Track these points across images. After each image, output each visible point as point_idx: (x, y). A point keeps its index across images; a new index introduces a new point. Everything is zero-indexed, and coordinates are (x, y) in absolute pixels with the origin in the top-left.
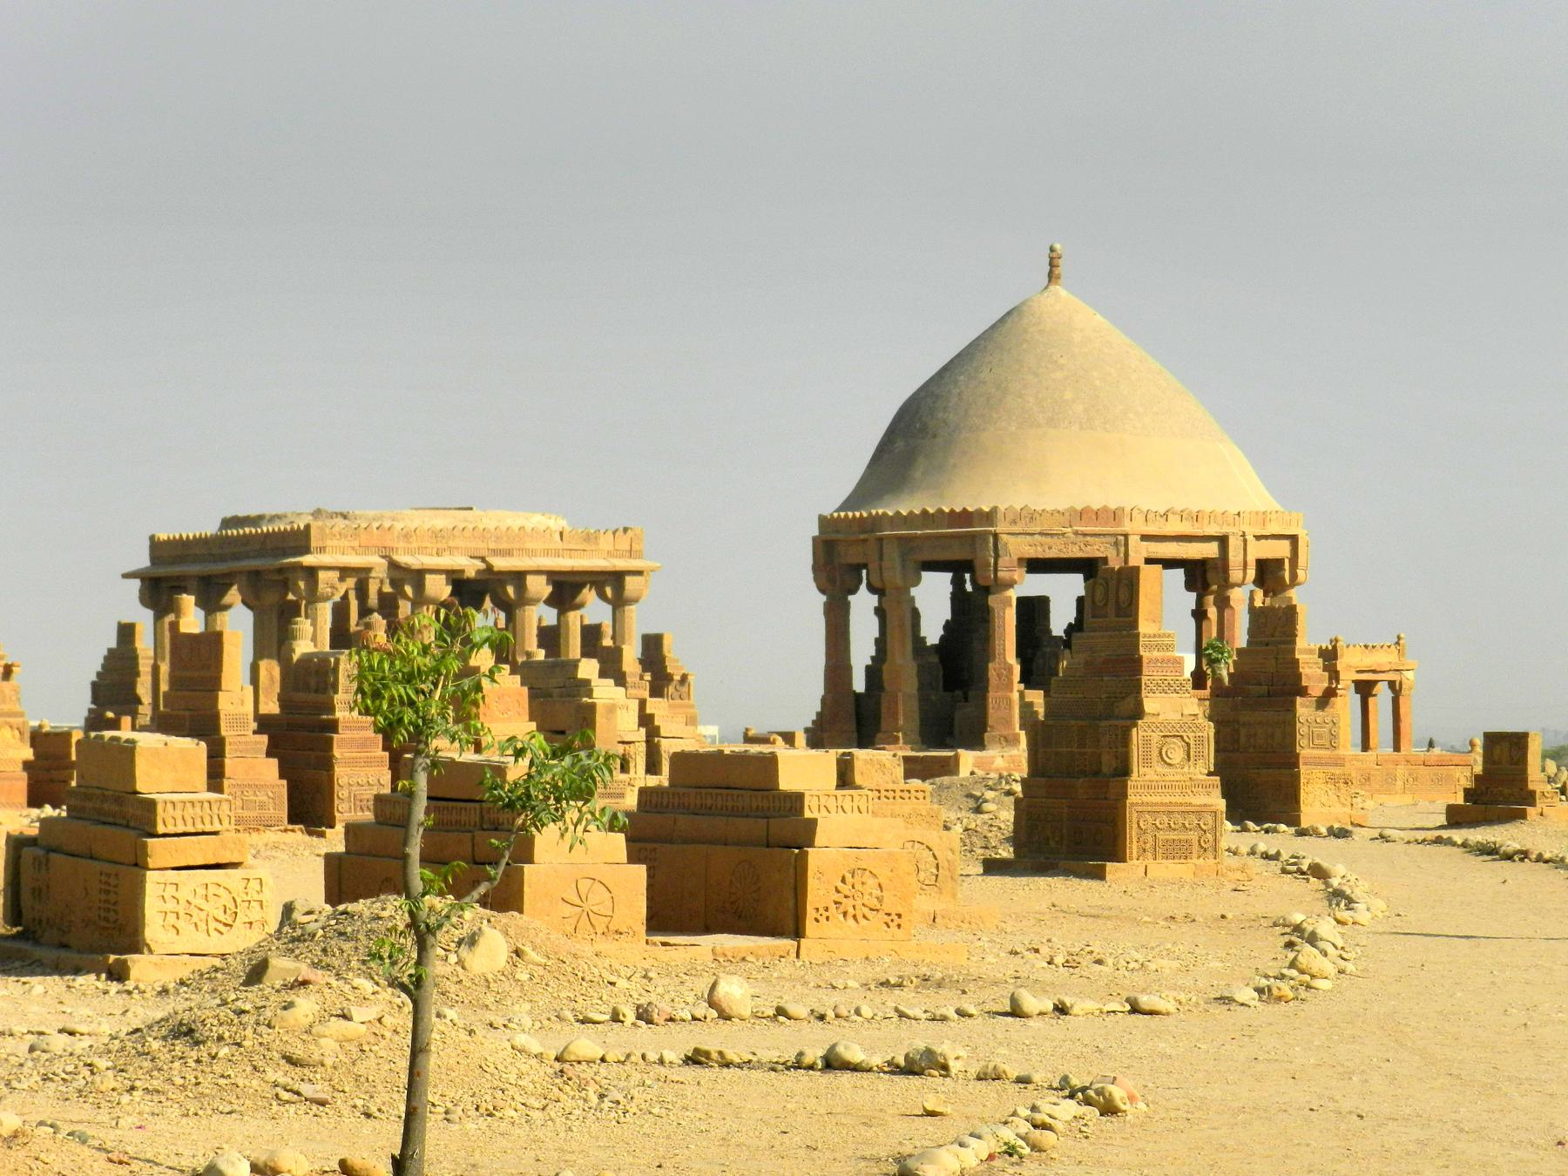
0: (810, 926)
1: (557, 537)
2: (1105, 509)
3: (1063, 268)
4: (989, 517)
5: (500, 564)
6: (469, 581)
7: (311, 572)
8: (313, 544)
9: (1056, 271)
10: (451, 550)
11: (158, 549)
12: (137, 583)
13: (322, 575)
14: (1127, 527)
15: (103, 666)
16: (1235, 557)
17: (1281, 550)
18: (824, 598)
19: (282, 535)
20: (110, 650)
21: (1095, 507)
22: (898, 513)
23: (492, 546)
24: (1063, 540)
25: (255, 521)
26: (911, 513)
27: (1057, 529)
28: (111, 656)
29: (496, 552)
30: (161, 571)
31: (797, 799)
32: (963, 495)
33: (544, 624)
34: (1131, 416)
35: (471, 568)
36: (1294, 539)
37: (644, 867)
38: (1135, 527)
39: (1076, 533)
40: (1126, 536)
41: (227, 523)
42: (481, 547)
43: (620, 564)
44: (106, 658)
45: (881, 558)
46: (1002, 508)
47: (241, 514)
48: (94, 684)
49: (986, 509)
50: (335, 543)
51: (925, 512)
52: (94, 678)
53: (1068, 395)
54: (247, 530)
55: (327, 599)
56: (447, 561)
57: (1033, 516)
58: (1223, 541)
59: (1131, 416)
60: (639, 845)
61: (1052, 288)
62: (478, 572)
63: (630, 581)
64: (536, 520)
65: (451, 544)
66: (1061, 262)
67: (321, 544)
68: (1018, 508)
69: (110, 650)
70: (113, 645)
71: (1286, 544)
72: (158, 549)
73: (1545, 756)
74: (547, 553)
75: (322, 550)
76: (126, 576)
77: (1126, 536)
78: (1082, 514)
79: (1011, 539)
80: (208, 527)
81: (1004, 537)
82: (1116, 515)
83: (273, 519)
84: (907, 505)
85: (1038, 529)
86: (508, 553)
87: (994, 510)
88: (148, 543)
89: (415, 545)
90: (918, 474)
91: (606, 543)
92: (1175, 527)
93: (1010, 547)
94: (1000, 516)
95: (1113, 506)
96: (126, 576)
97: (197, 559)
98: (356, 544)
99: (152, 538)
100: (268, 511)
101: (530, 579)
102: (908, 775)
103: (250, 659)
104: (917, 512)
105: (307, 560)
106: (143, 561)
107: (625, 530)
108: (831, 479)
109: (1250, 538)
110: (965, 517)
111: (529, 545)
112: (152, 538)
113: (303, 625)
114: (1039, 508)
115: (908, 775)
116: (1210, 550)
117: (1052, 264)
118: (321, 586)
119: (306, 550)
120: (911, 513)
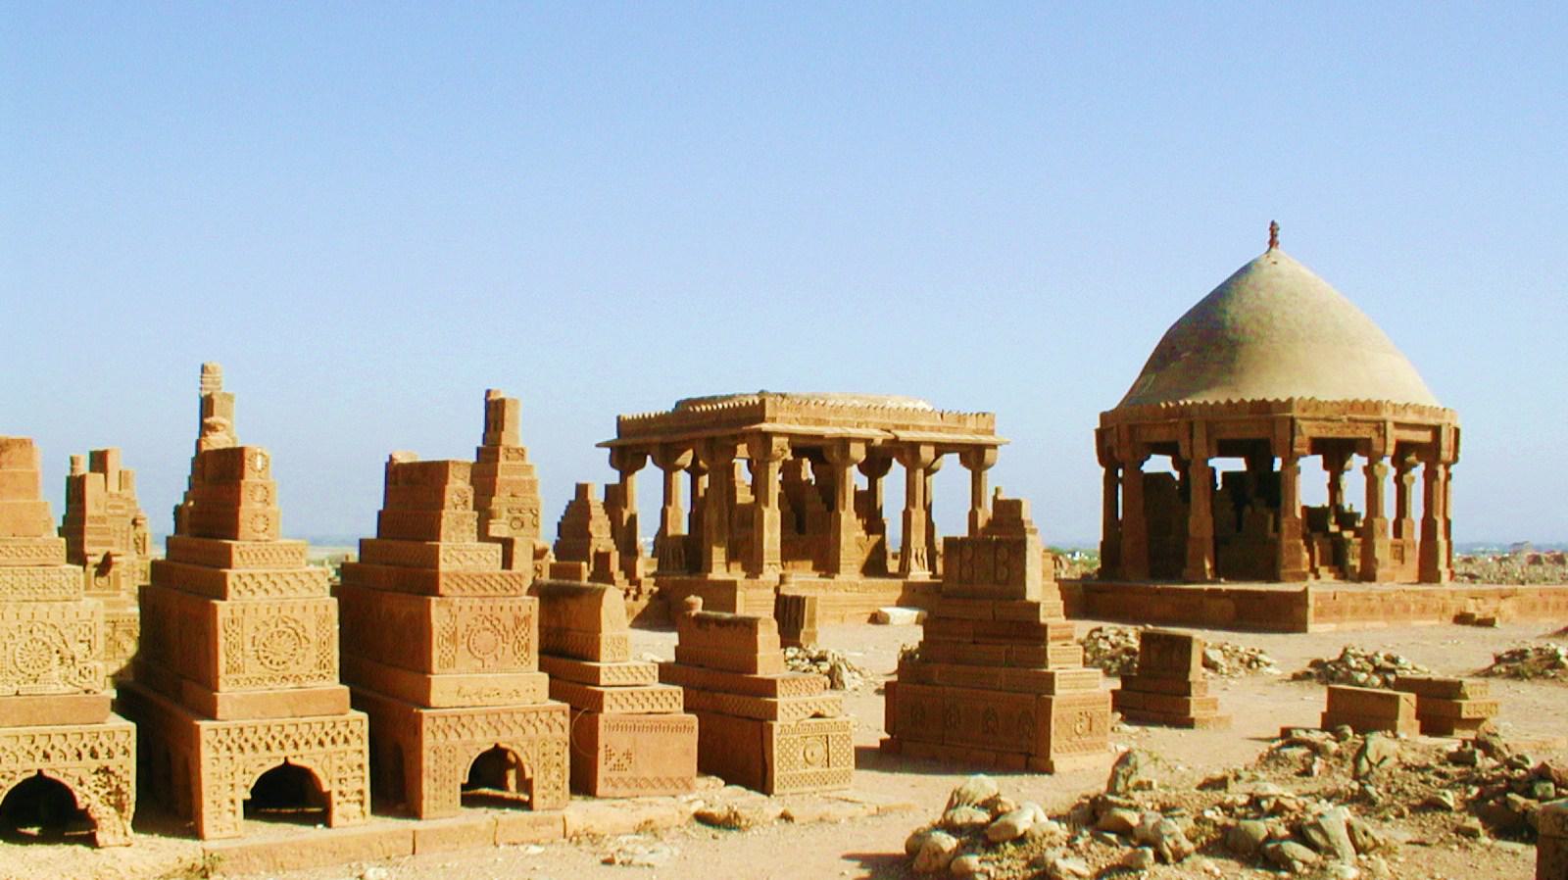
0: (239, 445)
1: (939, 417)
5: (904, 435)
7: (767, 436)
11: (622, 425)
12: (607, 451)
13: (775, 440)
15: (566, 512)
19: (737, 410)
20: (570, 502)
21: (1363, 399)
22: (1206, 403)
23: (896, 422)
24: (1340, 424)
25: (713, 400)
26: (1217, 403)
29: (897, 427)
30: (629, 441)
31: (1036, 607)
33: (859, 489)
35: (879, 437)
39: (1349, 419)
40: (1385, 422)
42: (890, 422)
43: (984, 439)
44: (568, 507)
45: (1191, 436)
46: (1297, 398)
48: (559, 524)
49: (1283, 400)
51: (1229, 402)
52: (559, 519)
56: (864, 432)
58: (1436, 430)
61: (1273, 250)
63: (988, 452)
64: (921, 405)
66: (1279, 232)
68: (1308, 398)
69: (570, 502)
70: (573, 498)
72: (622, 425)
74: (932, 429)
75: (774, 420)
76: (598, 445)
77: (1385, 422)
78: (1353, 406)
80: (667, 406)
81: (1299, 421)
82: (1377, 407)
85: (1322, 416)
86: (906, 428)
87: (1290, 400)
89: (841, 419)
91: (971, 424)
92: (1411, 418)
93: (1304, 429)
94: (1295, 406)
96: (598, 445)
97: (655, 432)
98: (799, 416)
99: (619, 418)
100: (737, 391)
101: (923, 449)
105: (765, 427)
106: (612, 435)
107: (984, 414)
108: (1113, 381)
110: (1262, 407)
111: (923, 423)
113: (706, 485)
114: (1323, 399)
115: (413, 812)
116: (1425, 437)
117: (1273, 235)
118: (774, 448)
119: (762, 420)
120: (1217, 403)
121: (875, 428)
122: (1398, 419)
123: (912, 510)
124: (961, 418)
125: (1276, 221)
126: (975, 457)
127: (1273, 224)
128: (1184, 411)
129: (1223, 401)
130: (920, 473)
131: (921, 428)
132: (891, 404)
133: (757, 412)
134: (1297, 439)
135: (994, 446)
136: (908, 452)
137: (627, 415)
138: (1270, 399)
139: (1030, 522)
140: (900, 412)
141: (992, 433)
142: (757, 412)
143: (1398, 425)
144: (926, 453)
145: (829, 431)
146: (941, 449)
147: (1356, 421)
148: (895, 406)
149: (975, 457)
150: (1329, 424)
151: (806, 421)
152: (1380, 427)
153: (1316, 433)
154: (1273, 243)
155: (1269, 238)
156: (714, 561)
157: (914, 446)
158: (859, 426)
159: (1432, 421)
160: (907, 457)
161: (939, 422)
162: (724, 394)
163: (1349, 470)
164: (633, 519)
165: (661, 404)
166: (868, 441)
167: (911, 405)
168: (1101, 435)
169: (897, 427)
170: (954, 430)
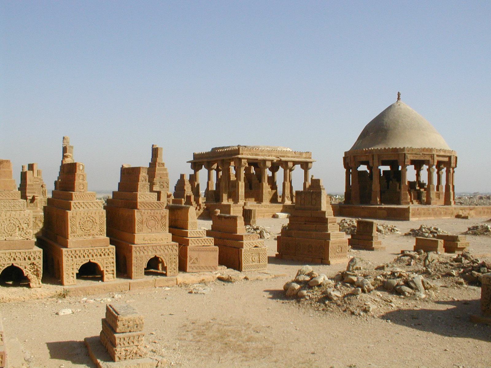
2: (429, 148)
5: (283, 159)
7: (240, 159)
8: (240, 152)
11: (195, 156)
12: (190, 164)
13: (243, 160)
19: (231, 151)
22: (378, 149)
23: (280, 155)
24: (420, 155)
25: (223, 148)
26: (381, 149)
27: (418, 153)
28: (179, 181)
29: (281, 156)
30: (197, 161)
31: (324, 213)
32: (393, 144)
35: (275, 159)
38: (434, 153)
39: (423, 154)
40: (434, 155)
43: (308, 160)
44: (178, 181)
45: (373, 159)
50: (245, 152)
51: (385, 149)
55: (244, 166)
56: (270, 158)
58: (450, 157)
60: (171, 229)
63: (309, 164)
64: (288, 149)
65: (272, 154)
67: (242, 153)
70: (179, 179)
72: (195, 156)
73: (412, 210)
74: (292, 157)
75: (242, 154)
76: (155, 152)
77: (434, 155)
79: (409, 155)
81: (407, 154)
82: (431, 150)
84: (379, 147)
86: (283, 157)
87: (404, 148)
88: (193, 154)
91: (304, 156)
92: (442, 153)
93: (408, 157)
94: (405, 149)
96: (187, 162)
98: (250, 153)
99: (194, 153)
100: (231, 145)
104: (383, 148)
105: (240, 156)
106: (192, 159)
110: (395, 150)
111: (289, 155)
114: (414, 148)
116: (446, 159)
118: (242, 163)
119: (239, 154)
120: (381, 149)
122: (438, 154)
124: (301, 154)
126: (305, 166)
130: (288, 171)
131: (288, 157)
133: (237, 152)
135: (311, 162)
136: (284, 164)
138: (398, 148)
139: (323, 186)
140: (282, 152)
141: (311, 158)
142: (237, 152)
143: (438, 156)
144: (290, 165)
145: (260, 158)
146: (295, 163)
147: (425, 154)
148: (280, 150)
149: (305, 166)
150: (416, 155)
151: (252, 155)
152: (432, 156)
153: (412, 158)
157: (286, 162)
158: (269, 156)
159: (449, 154)
161: (294, 155)
163: (422, 170)
166: (272, 161)
167: (285, 149)
168: (345, 159)
169: (281, 156)
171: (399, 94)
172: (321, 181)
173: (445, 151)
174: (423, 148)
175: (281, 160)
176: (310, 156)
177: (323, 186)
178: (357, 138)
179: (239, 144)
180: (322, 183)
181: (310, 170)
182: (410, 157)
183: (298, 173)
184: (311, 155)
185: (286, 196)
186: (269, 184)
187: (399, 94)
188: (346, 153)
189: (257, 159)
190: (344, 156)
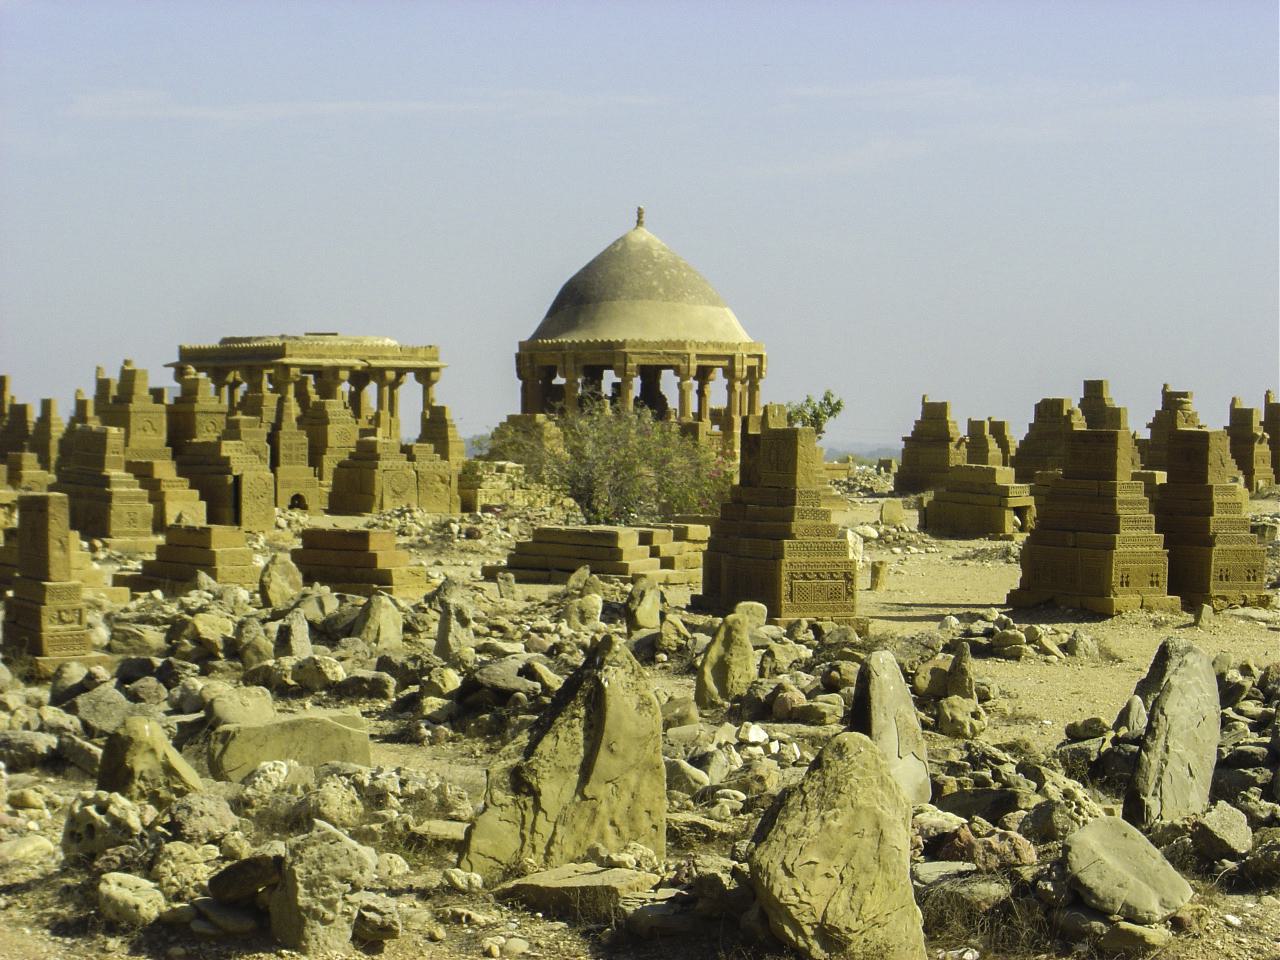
2: (678, 341)
3: (645, 218)
4: (622, 344)
5: (375, 363)
6: (358, 372)
7: (287, 367)
9: (642, 220)
10: (351, 357)
13: (292, 369)
14: (689, 350)
16: (738, 366)
17: (755, 362)
18: (520, 382)
19: (268, 348)
22: (573, 341)
23: (371, 355)
25: (248, 340)
26: (581, 341)
29: (370, 358)
34: (686, 294)
35: (358, 364)
36: (760, 357)
37: (605, 371)
39: (665, 353)
41: (225, 341)
43: (430, 364)
47: (237, 336)
49: (621, 340)
53: (655, 283)
54: (244, 345)
57: (643, 344)
59: (686, 294)
62: (363, 367)
63: (434, 375)
64: (389, 342)
66: (644, 215)
71: (757, 360)
74: (394, 358)
75: (291, 356)
76: (166, 366)
77: (689, 354)
80: (1027, 431)
81: (629, 355)
82: (682, 344)
83: (259, 339)
90: (580, 322)
91: (421, 354)
92: (711, 351)
95: (682, 340)
96: (166, 366)
102: (114, 585)
103: (422, 410)
104: (584, 341)
105: (286, 360)
109: (745, 356)
111: (389, 355)
112: (969, 420)
114: (647, 340)
115: (114, 585)
119: (283, 355)
120: (581, 341)
121: (356, 358)
122: (700, 352)
123: (381, 412)
124: (414, 351)
125: (642, 207)
126: (425, 376)
127: (639, 209)
128: (560, 347)
129: (584, 341)
130: (386, 389)
131: (386, 358)
132: (367, 343)
133: (280, 352)
134: (629, 364)
135: (437, 369)
136: (377, 374)
137: (187, 346)
138: (613, 340)
139: (1111, 399)
140: (373, 348)
141: (436, 359)
142: (280, 352)
143: (699, 357)
144: (391, 375)
145: (326, 362)
146: (401, 372)
147: (669, 354)
148: (369, 344)
149: (425, 376)
150: (651, 356)
151: (311, 356)
152: (685, 358)
153: (643, 362)
154: (639, 223)
155: (636, 218)
156: (700, 571)
157: (381, 371)
158: (345, 358)
159: (728, 352)
160: (378, 377)
161: (400, 354)
162: (257, 336)
163: (712, 380)
164: (238, 480)
165: (210, 341)
166: (350, 368)
167: (380, 343)
168: (519, 358)
169: (370, 358)
170: (410, 358)
171: (640, 213)
172: (447, 411)
173: (719, 345)
174: (666, 340)
175: (369, 367)
176: (435, 356)
177: (452, 421)
178: (549, 306)
179: (284, 333)
180: (449, 416)
181: (435, 385)
182: (634, 362)
183: (410, 393)
184: (436, 351)
185: (378, 501)
186: (1232, 458)
187: (640, 213)
188: (522, 345)
189: (320, 366)
190: (517, 351)
